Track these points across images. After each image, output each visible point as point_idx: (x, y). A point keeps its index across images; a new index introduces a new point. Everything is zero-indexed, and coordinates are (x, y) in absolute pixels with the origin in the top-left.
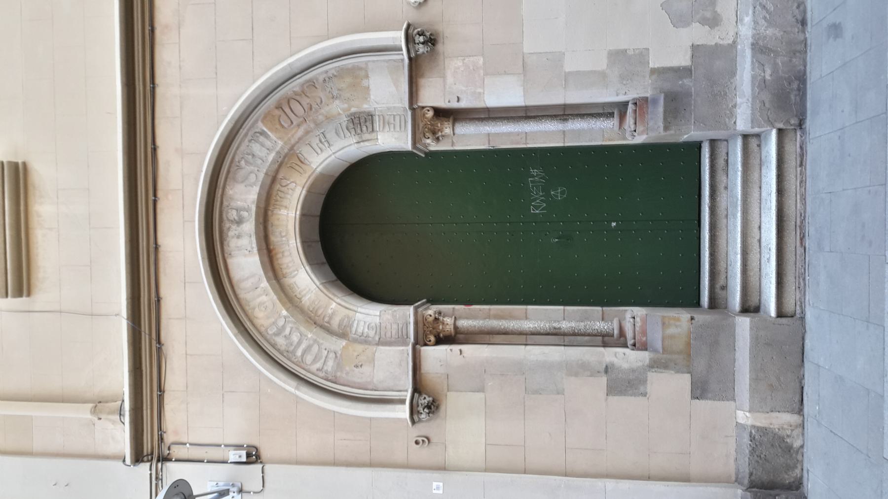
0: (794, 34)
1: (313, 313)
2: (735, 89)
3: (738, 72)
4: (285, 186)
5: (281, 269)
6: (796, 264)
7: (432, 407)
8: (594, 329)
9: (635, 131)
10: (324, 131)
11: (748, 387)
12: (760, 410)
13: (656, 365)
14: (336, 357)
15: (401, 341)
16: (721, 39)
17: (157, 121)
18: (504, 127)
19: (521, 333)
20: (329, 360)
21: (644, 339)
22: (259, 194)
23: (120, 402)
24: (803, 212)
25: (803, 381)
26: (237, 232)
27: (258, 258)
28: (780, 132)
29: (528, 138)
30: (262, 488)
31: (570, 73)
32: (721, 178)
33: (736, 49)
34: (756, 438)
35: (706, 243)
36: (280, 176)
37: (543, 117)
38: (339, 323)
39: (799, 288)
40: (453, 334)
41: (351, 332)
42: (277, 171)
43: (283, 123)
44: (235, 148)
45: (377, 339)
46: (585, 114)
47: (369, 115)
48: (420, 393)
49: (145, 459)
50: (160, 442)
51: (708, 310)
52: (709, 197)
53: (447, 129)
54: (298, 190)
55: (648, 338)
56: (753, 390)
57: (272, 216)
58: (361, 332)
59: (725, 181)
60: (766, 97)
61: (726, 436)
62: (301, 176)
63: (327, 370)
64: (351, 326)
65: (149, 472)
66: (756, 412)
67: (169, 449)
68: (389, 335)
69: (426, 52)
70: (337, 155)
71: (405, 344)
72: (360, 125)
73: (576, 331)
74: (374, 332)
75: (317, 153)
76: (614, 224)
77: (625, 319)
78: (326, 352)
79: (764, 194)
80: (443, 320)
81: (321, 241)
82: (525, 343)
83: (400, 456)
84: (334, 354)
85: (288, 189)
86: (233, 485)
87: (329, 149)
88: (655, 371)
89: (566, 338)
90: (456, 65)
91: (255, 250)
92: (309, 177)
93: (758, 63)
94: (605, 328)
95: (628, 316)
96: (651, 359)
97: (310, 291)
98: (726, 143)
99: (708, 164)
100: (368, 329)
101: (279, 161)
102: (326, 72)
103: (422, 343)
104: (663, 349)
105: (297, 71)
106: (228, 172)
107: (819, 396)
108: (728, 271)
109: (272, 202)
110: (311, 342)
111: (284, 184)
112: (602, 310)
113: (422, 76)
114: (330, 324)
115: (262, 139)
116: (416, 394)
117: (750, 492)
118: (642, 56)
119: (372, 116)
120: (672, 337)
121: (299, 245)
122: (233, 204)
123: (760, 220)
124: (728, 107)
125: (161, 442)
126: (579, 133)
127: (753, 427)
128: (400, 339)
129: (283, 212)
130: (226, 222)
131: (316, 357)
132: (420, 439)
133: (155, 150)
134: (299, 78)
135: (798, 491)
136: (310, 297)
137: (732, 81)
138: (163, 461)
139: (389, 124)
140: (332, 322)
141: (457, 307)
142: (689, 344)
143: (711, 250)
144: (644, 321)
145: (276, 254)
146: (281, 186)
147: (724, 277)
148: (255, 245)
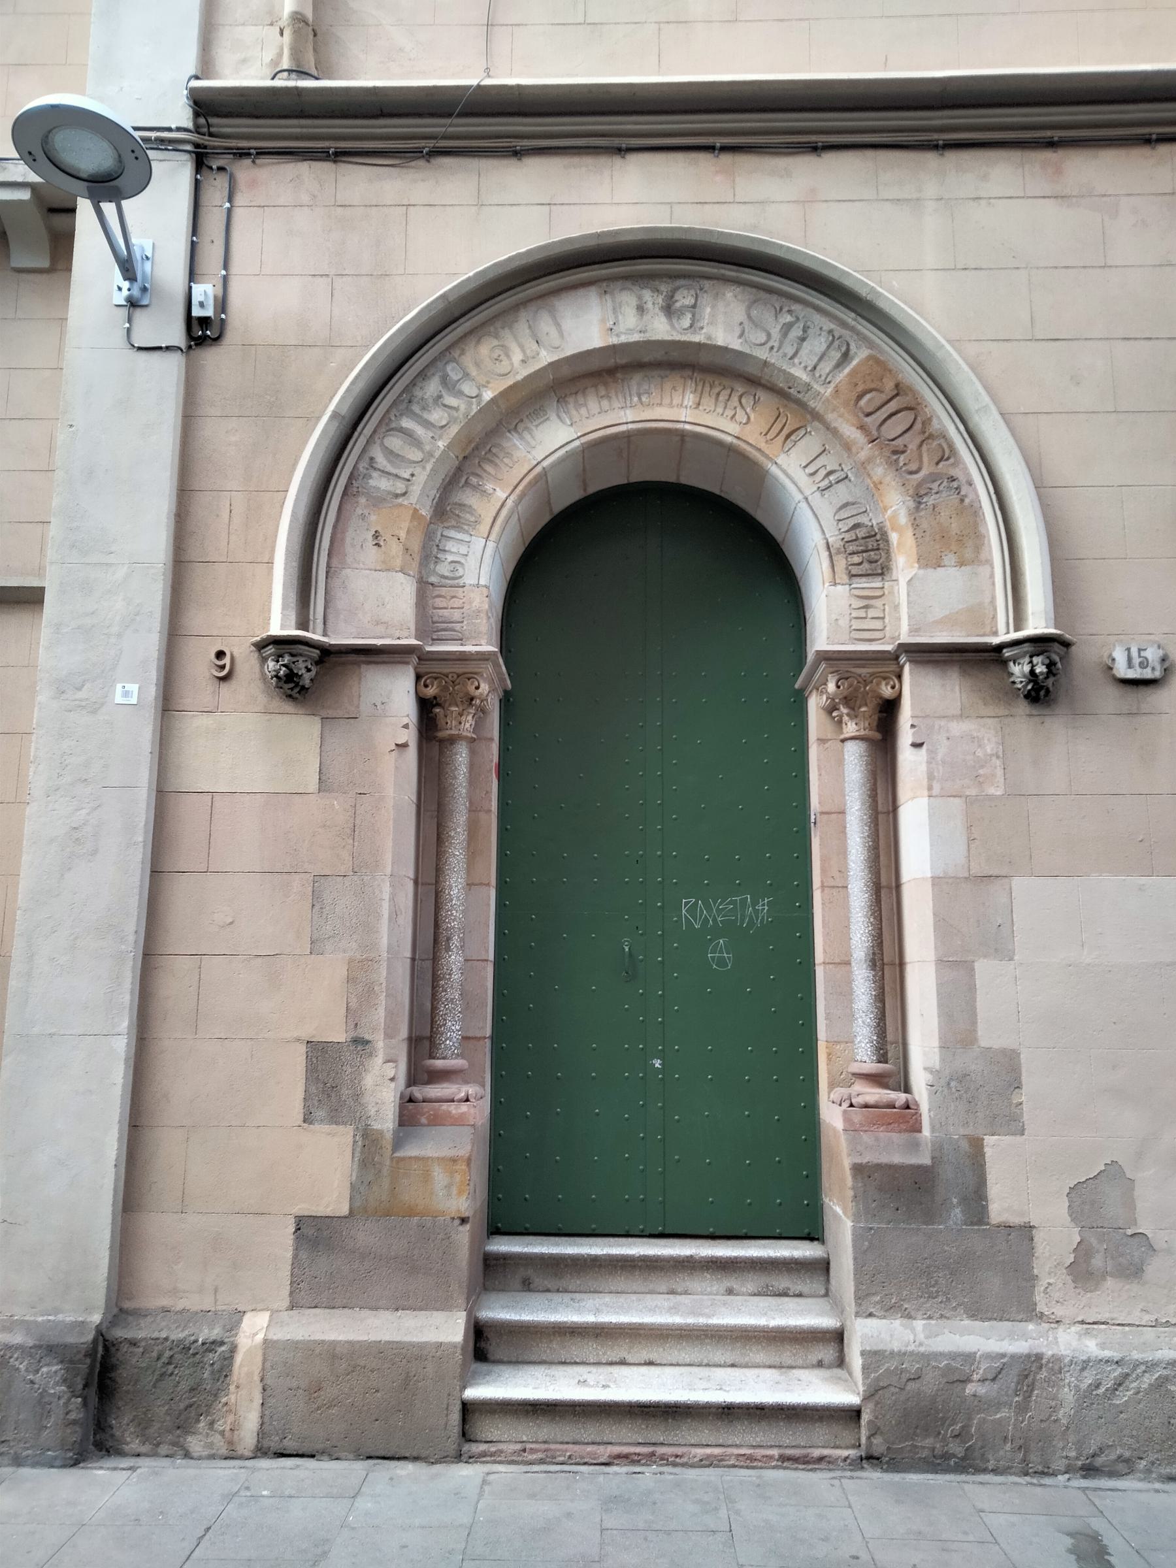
0: (1063, 1449)
1: (486, 454)
2: (942, 1316)
3: (978, 1323)
4: (740, 403)
5: (576, 393)
6: (574, 1443)
7: (291, 685)
8: (445, 1020)
9: (851, 1105)
10: (850, 480)
11: (319, 1337)
12: (268, 1364)
13: (368, 1141)
14: (397, 496)
15: (427, 623)
16: (1047, 1288)
17: (870, 153)
18: (858, 839)
19: (439, 871)
20: (391, 481)
21: (424, 1120)
22: (725, 350)
23: (316, 75)
24: (684, 1460)
25: (326, 1458)
26: (650, 305)
27: (597, 346)
28: (854, 1414)
29: (835, 891)
30: (136, 345)
31: (971, 971)
32: (751, 1283)
33: (1026, 1321)
34: (211, 1355)
35: (619, 1249)
36: (762, 395)
37: (879, 918)
38: (464, 505)
39: (524, 1450)
40: (441, 734)
41: (447, 528)
42: (772, 389)
43: (868, 396)
44: (818, 302)
45: (433, 579)
46: (884, 1004)
47: (882, 568)
48: (319, 662)
49: (202, 121)
50: (235, 151)
51: (482, 1251)
52: (712, 1257)
53: (854, 726)
54: (733, 428)
55: (425, 1128)
56: (309, 1349)
57: (682, 377)
58: (447, 548)
59: (744, 1289)
60: (930, 1384)
61: (216, 1290)
62: (761, 433)
63: (370, 477)
64: (458, 528)
65: (173, 126)
66: (264, 1354)
67: (221, 169)
68: (439, 602)
69: (1012, 680)
70: (804, 505)
71: (420, 633)
72: (863, 552)
73: (442, 982)
74: (446, 574)
75: (805, 467)
76: (657, 1063)
77: (466, 1082)
78: (407, 476)
79: (719, 1373)
80: (469, 713)
81: (629, 485)
82: (420, 880)
83: (196, 620)
84: (404, 491)
85: (735, 408)
86: (144, 290)
87: (816, 489)
88: (355, 1142)
89: (429, 964)
90: (986, 741)
91: (614, 340)
92: (759, 450)
93: (1002, 1367)
94: (448, 1042)
95: (472, 1090)
96: (381, 1133)
97: (529, 450)
98: (823, 1292)
99: (779, 1255)
100: (452, 562)
101: (792, 391)
102: (970, 483)
103: (422, 670)
104: (403, 1159)
105: (971, 425)
106: (770, 290)
107: (290, 1497)
108: (561, 1294)
109: (709, 378)
110: (427, 448)
111: (743, 401)
112: (485, 1038)
113: (964, 673)
114: (463, 487)
115: (836, 355)
116: (318, 652)
117: (95, 1341)
118: (1012, 1123)
119: (882, 574)
120: (427, 1177)
121: (623, 428)
122: (706, 301)
123: (665, 1365)
124: (903, 1300)
125: (234, 154)
126: (844, 992)
127: (233, 1349)
128: (431, 624)
129: (690, 398)
130: (671, 285)
131: (398, 455)
132: (227, 661)
133: (815, 149)
134: (957, 428)
135: (91, 1447)
136: (519, 449)
137: (961, 1310)
138: (197, 154)
139: (866, 607)
140: (468, 491)
141: (495, 747)
142: (411, 1212)
143: (605, 1260)
144: (459, 1121)
145: (606, 384)
146: (741, 397)
147: (549, 1286)
148: (623, 339)
